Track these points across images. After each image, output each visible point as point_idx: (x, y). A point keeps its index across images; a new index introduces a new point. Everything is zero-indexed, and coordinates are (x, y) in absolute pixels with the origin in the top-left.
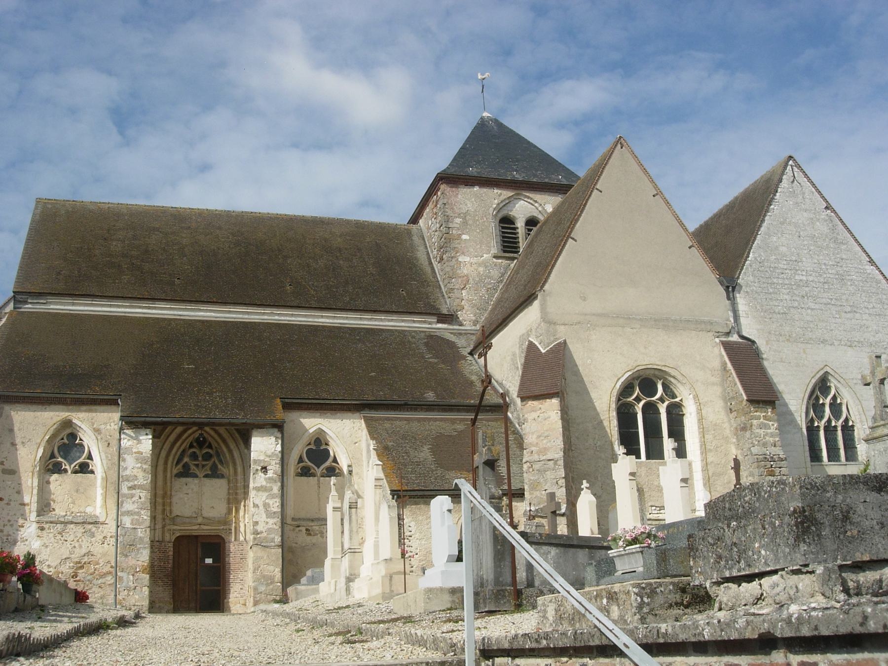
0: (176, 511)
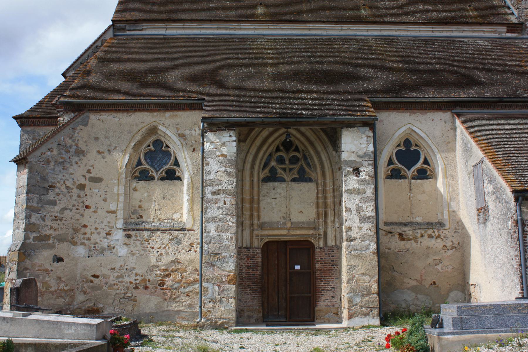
0: (265, 217)
